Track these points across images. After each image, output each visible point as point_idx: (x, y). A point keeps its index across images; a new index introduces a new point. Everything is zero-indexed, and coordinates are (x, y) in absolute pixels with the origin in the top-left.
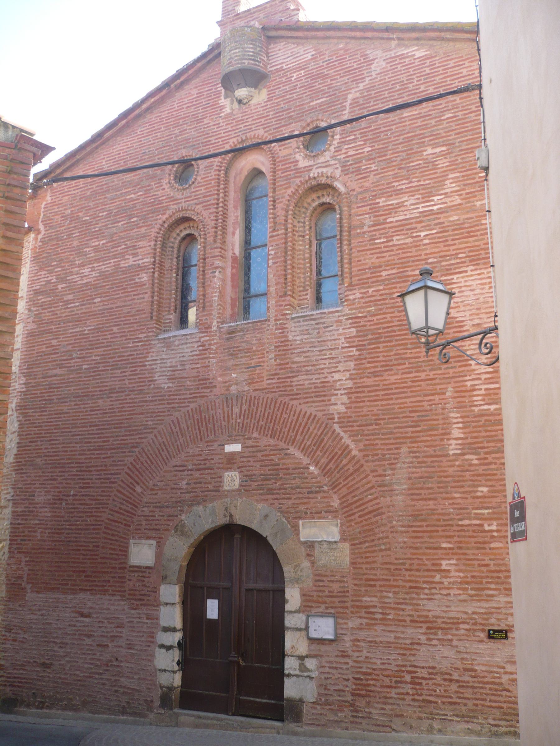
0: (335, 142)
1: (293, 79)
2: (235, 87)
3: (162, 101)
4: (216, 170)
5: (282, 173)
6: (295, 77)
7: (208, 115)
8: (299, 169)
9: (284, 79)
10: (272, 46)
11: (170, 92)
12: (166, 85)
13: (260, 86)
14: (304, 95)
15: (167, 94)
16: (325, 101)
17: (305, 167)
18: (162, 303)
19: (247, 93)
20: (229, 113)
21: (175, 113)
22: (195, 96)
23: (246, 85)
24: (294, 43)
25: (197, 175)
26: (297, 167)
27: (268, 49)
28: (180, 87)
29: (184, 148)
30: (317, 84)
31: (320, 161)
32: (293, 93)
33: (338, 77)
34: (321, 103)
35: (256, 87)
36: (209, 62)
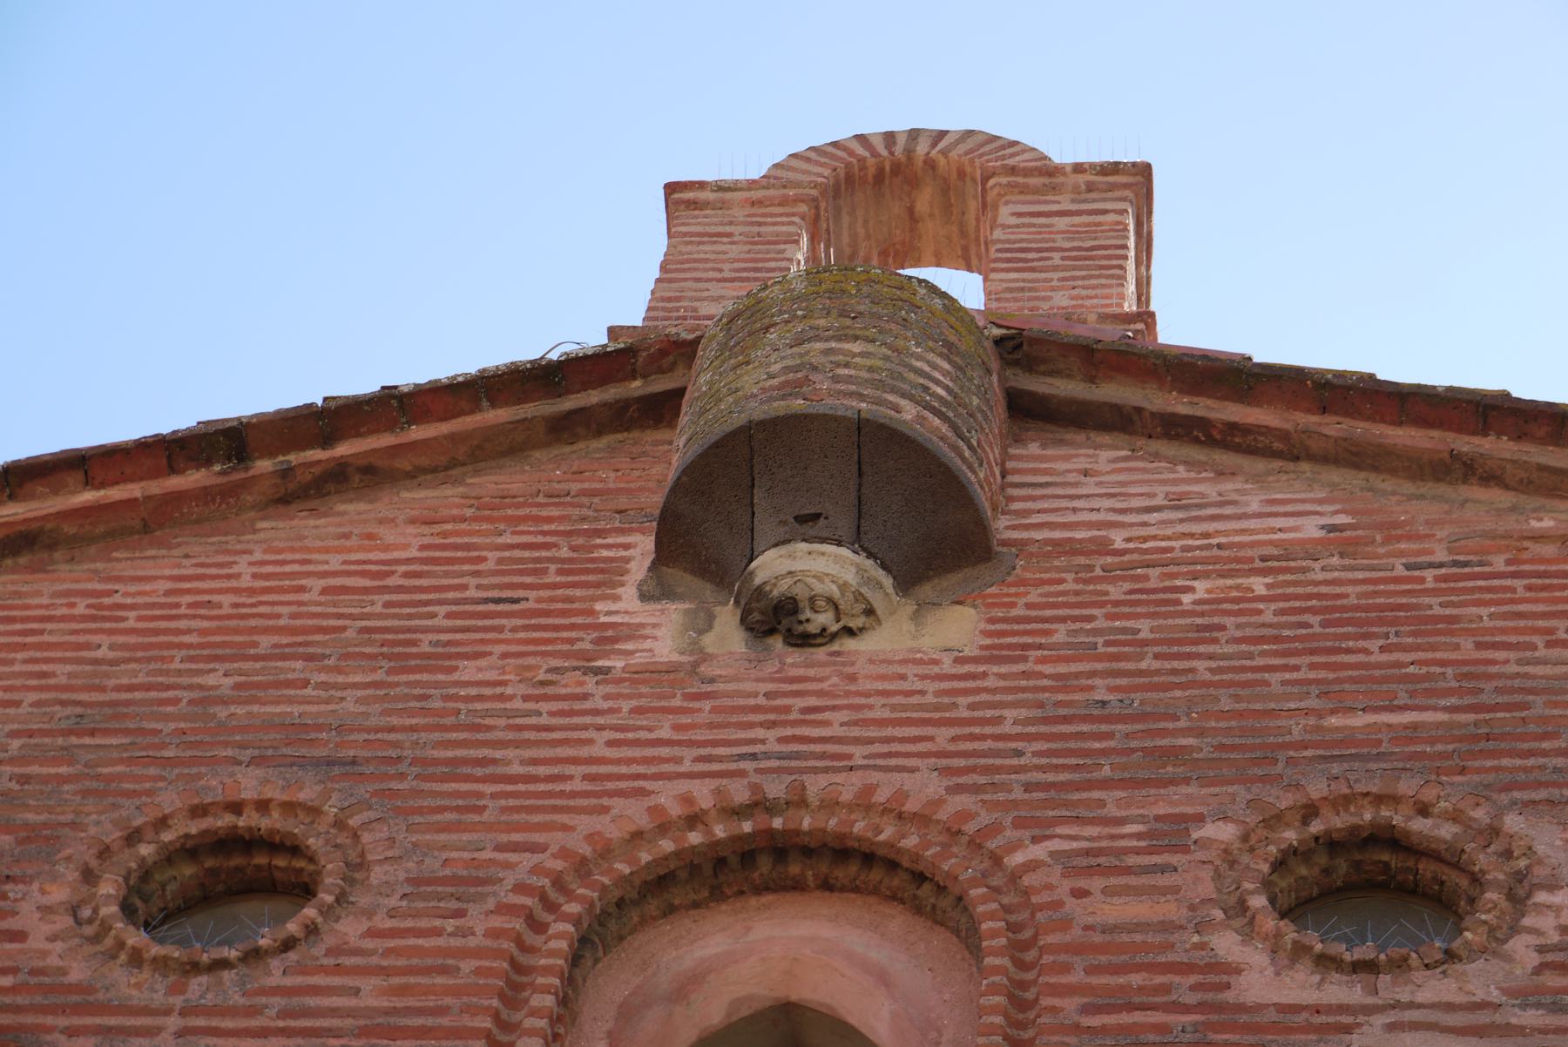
0: (1520, 946)
1: (1187, 599)
2: (765, 525)
3: (151, 523)
4: (504, 909)
5: (1086, 1010)
6: (1200, 594)
7: (498, 649)
8: (1241, 1008)
9: (1116, 592)
10: (1034, 448)
11: (228, 493)
12: (227, 442)
13: (927, 590)
14: (1275, 678)
15: (205, 495)
16: (1439, 725)
17: (1282, 1008)
18: (501, 996)
19: (850, 576)
20: (672, 669)
21: (227, 600)
22: (413, 553)
23: (858, 540)
24: (1188, 463)
25: (326, 911)
26: (1229, 996)
27: (1005, 457)
28: (298, 493)
29: (255, 761)
30: (1374, 645)
31: (1421, 997)
32: (1198, 656)
33: (1538, 640)
34: (1415, 726)
35: (907, 582)
36: (563, 429)
